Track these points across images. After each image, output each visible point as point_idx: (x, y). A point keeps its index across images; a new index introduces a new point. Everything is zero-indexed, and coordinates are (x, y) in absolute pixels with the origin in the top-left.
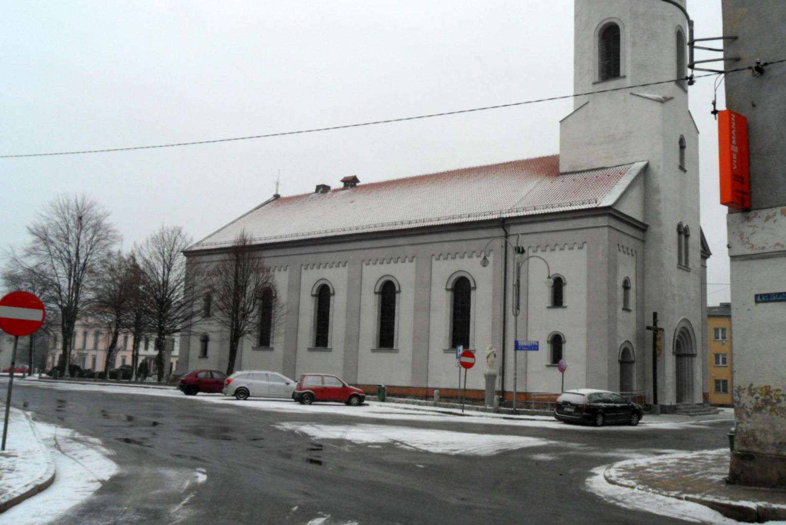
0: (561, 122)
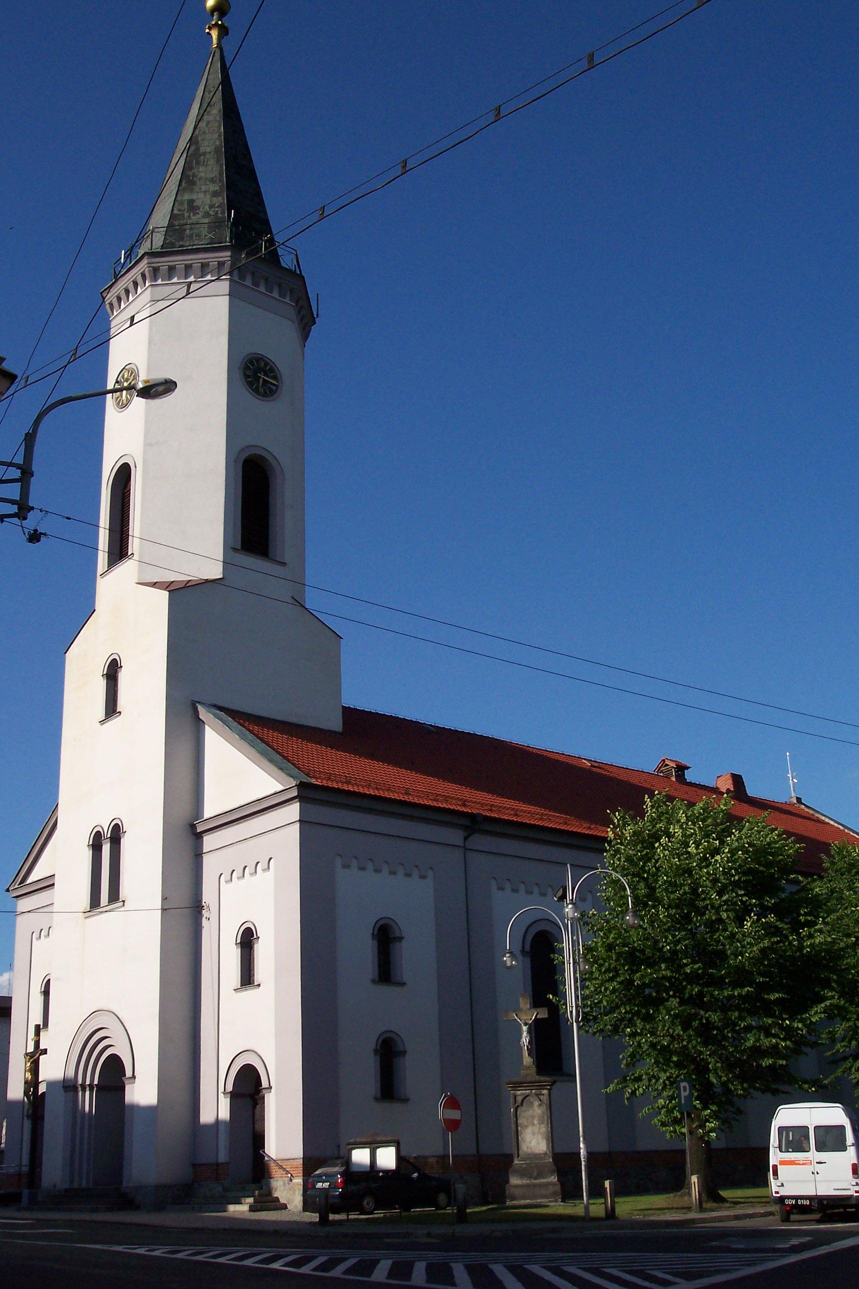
0: (95, 610)
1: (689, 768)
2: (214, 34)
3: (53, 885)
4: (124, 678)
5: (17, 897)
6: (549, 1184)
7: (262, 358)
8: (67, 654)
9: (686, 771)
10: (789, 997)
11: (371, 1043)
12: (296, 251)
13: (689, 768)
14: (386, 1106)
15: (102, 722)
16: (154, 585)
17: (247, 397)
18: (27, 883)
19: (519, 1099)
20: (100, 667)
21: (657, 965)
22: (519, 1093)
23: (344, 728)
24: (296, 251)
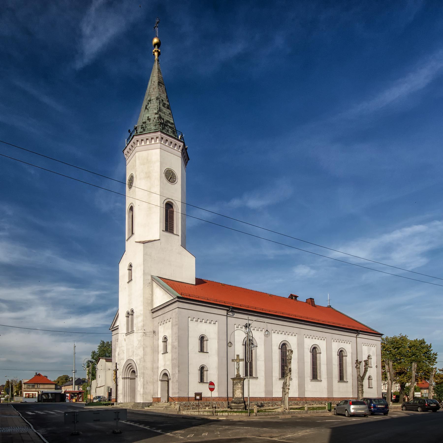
0: (125, 251)
1: (298, 297)
2: (156, 54)
3: (118, 328)
4: (133, 269)
5: (112, 331)
6: (242, 405)
7: (171, 170)
8: (119, 264)
9: (297, 298)
10: (187, 437)
11: (198, 367)
12: (181, 133)
13: (298, 297)
14: (201, 384)
15: (384, 335)
16: (140, 242)
17: (165, 181)
18: (115, 326)
19: (235, 383)
20: (127, 267)
21: (66, 397)
22: (235, 381)
23: (196, 284)
24: (181, 133)
